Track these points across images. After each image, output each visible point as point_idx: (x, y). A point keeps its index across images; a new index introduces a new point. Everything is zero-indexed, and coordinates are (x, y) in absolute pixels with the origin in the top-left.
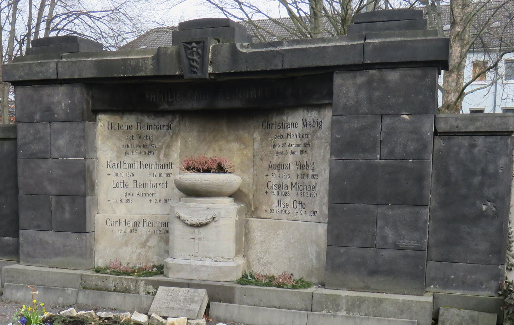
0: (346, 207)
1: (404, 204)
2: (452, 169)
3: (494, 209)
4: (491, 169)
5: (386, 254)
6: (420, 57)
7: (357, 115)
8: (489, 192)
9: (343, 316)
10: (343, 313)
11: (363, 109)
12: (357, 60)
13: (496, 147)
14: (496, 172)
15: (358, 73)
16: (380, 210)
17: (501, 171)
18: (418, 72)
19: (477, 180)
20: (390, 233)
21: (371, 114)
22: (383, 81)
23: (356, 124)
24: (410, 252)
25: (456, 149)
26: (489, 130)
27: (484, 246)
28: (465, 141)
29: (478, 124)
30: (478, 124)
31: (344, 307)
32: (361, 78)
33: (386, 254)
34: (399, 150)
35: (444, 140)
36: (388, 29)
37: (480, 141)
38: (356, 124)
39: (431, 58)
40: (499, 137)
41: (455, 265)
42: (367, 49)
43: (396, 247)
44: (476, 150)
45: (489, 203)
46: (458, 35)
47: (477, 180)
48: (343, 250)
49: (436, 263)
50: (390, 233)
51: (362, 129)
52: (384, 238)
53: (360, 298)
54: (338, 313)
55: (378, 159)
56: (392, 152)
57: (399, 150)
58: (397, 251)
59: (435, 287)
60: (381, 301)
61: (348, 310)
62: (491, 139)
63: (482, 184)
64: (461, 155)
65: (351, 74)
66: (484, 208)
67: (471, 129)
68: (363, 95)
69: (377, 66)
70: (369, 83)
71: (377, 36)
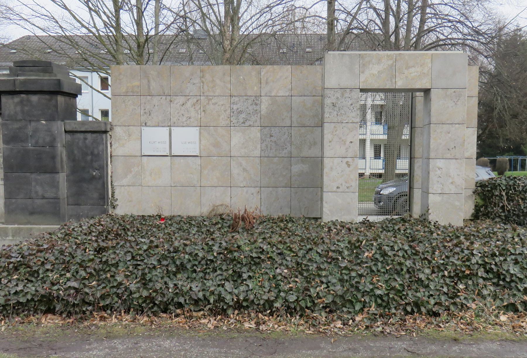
0: (14, 175)
1: (46, 172)
2: (76, 152)
3: (99, 174)
4: (96, 152)
5: (39, 202)
6: (46, 89)
7: (17, 120)
8: (96, 165)
9: (9, 240)
10: (11, 238)
11: (20, 117)
12: (10, 88)
13: (97, 139)
14: (98, 154)
15: (15, 96)
16: (33, 176)
17: (101, 153)
18: (47, 97)
19: (89, 158)
20: (39, 189)
21: (24, 120)
22: (29, 101)
23: (16, 125)
24: (51, 200)
25: (77, 140)
26: (92, 130)
27: (96, 195)
28: (81, 136)
29: (86, 127)
30: (86, 127)
31: (11, 234)
32: (17, 99)
33: (39, 202)
34: (41, 141)
35: (70, 135)
36: (32, 71)
37: (89, 136)
38: (16, 125)
39: (52, 90)
40: (98, 134)
41: (82, 207)
42: (16, 83)
43: (43, 198)
44: (87, 141)
45: (96, 171)
46: (227, 60)
47: (89, 158)
48: (14, 201)
49: (72, 206)
50: (39, 189)
51: (20, 128)
52: (36, 192)
53: (19, 228)
54: (8, 238)
55: (30, 146)
56: (37, 142)
57: (41, 141)
58: (44, 200)
59: (72, 220)
60: (31, 229)
61: (13, 236)
62: (94, 135)
63: (92, 160)
64: (80, 144)
65: (10, 96)
66: (94, 173)
67: (83, 129)
68: (18, 109)
69: (25, 93)
70: (21, 102)
71: (24, 75)
